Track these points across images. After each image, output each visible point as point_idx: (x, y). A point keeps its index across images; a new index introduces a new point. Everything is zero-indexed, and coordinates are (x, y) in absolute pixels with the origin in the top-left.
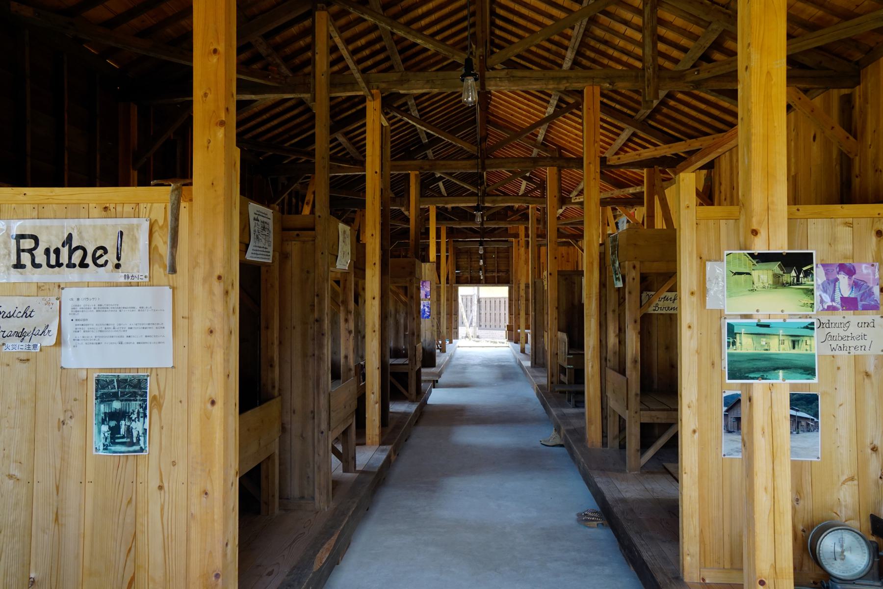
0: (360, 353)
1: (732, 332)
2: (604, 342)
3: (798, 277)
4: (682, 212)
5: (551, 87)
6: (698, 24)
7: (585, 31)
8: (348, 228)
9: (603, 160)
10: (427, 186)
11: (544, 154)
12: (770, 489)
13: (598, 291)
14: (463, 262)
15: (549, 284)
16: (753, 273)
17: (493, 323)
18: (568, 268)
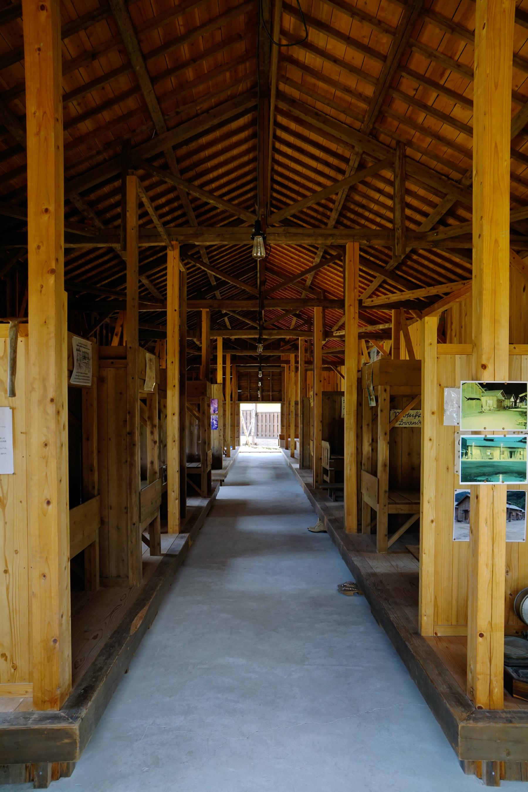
0: (162, 459)
1: (465, 445)
2: (360, 450)
3: (515, 402)
4: (426, 348)
5: (319, 242)
6: (436, 195)
7: (347, 196)
8: (153, 357)
9: (360, 302)
10: (216, 323)
11: (312, 296)
12: (490, 566)
13: (356, 409)
14: (244, 383)
15: (315, 403)
16: (482, 398)
17: (271, 434)
18: (329, 389)
